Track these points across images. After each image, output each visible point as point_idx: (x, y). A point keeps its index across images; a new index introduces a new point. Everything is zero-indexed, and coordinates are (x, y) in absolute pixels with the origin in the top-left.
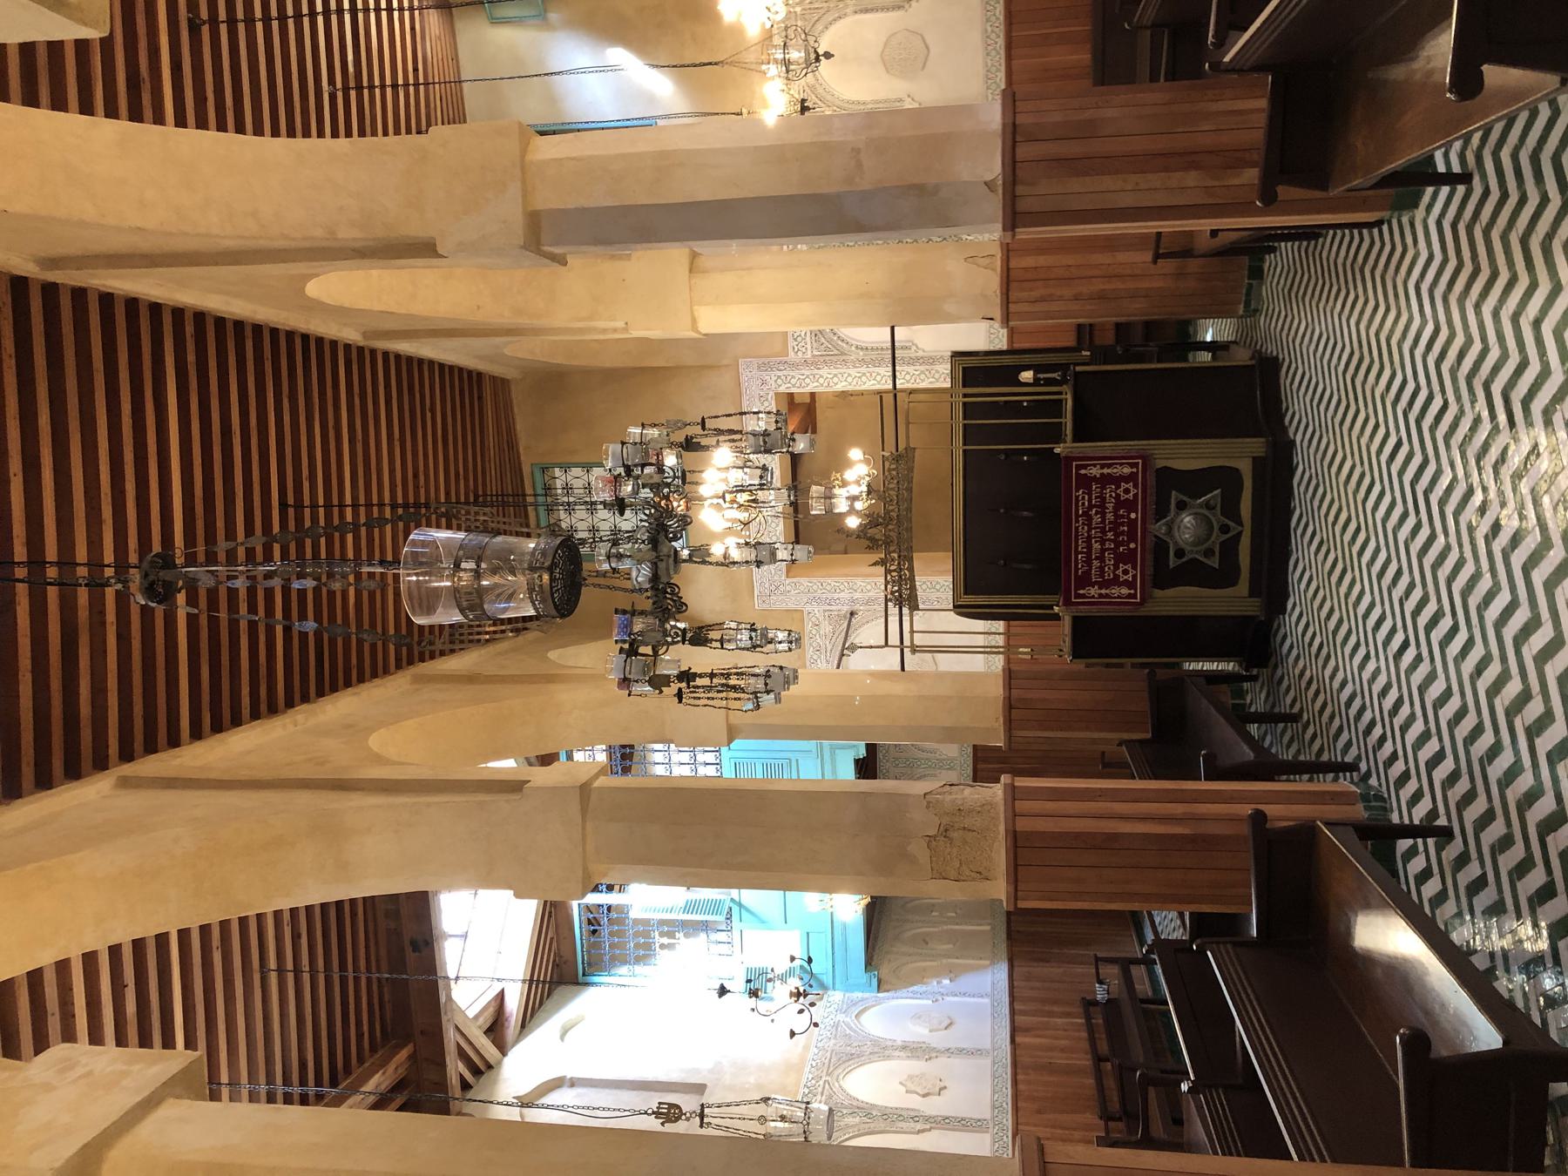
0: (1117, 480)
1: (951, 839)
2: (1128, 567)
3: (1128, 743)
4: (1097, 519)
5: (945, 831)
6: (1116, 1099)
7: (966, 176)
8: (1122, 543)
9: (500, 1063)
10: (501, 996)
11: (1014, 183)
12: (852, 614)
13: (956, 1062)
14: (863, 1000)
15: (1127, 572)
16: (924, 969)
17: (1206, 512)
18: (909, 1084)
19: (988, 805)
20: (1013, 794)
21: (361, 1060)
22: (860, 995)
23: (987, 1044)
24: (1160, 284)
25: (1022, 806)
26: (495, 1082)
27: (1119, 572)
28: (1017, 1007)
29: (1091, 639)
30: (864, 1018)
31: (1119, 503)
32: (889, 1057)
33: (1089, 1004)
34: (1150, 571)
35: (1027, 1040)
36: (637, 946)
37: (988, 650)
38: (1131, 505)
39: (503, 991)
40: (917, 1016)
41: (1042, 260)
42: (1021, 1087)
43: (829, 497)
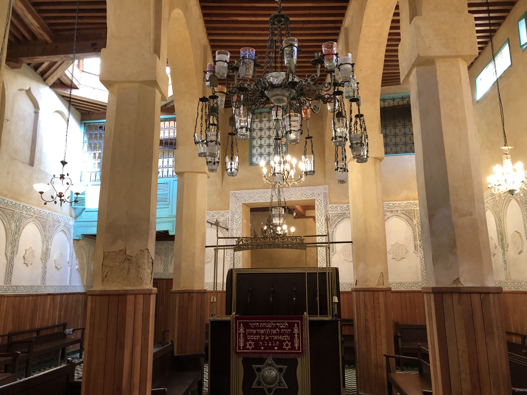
0: (292, 341)
1: (124, 262)
2: (253, 346)
3: (173, 345)
4: (274, 332)
5: (128, 259)
6: (18, 339)
7: (462, 269)
8: (263, 343)
9: (47, 84)
10: (76, 88)
11: (364, 291)
12: (227, 229)
13: (40, 271)
14: (70, 233)
15: (250, 346)
16: (83, 258)
17: (278, 381)
18: (29, 251)
19: (140, 279)
20: (147, 294)
21: (45, 18)
22: (72, 232)
23: (48, 283)
24: (373, 357)
25: (140, 298)
26: (38, 81)
27: (250, 342)
28: (64, 296)
29: (219, 329)
30: (62, 234)
31: (281, 342)
32: (43, 242)
33: (65, 326)
34: (251, 356)
35: (48, 302)
36: (95, 144)
37: (215, 284)
38: (280, 347)
39: (78, 88)
40: (61, 255)
41: (382, 306)
42: (26, 298)
43: (280, 216)
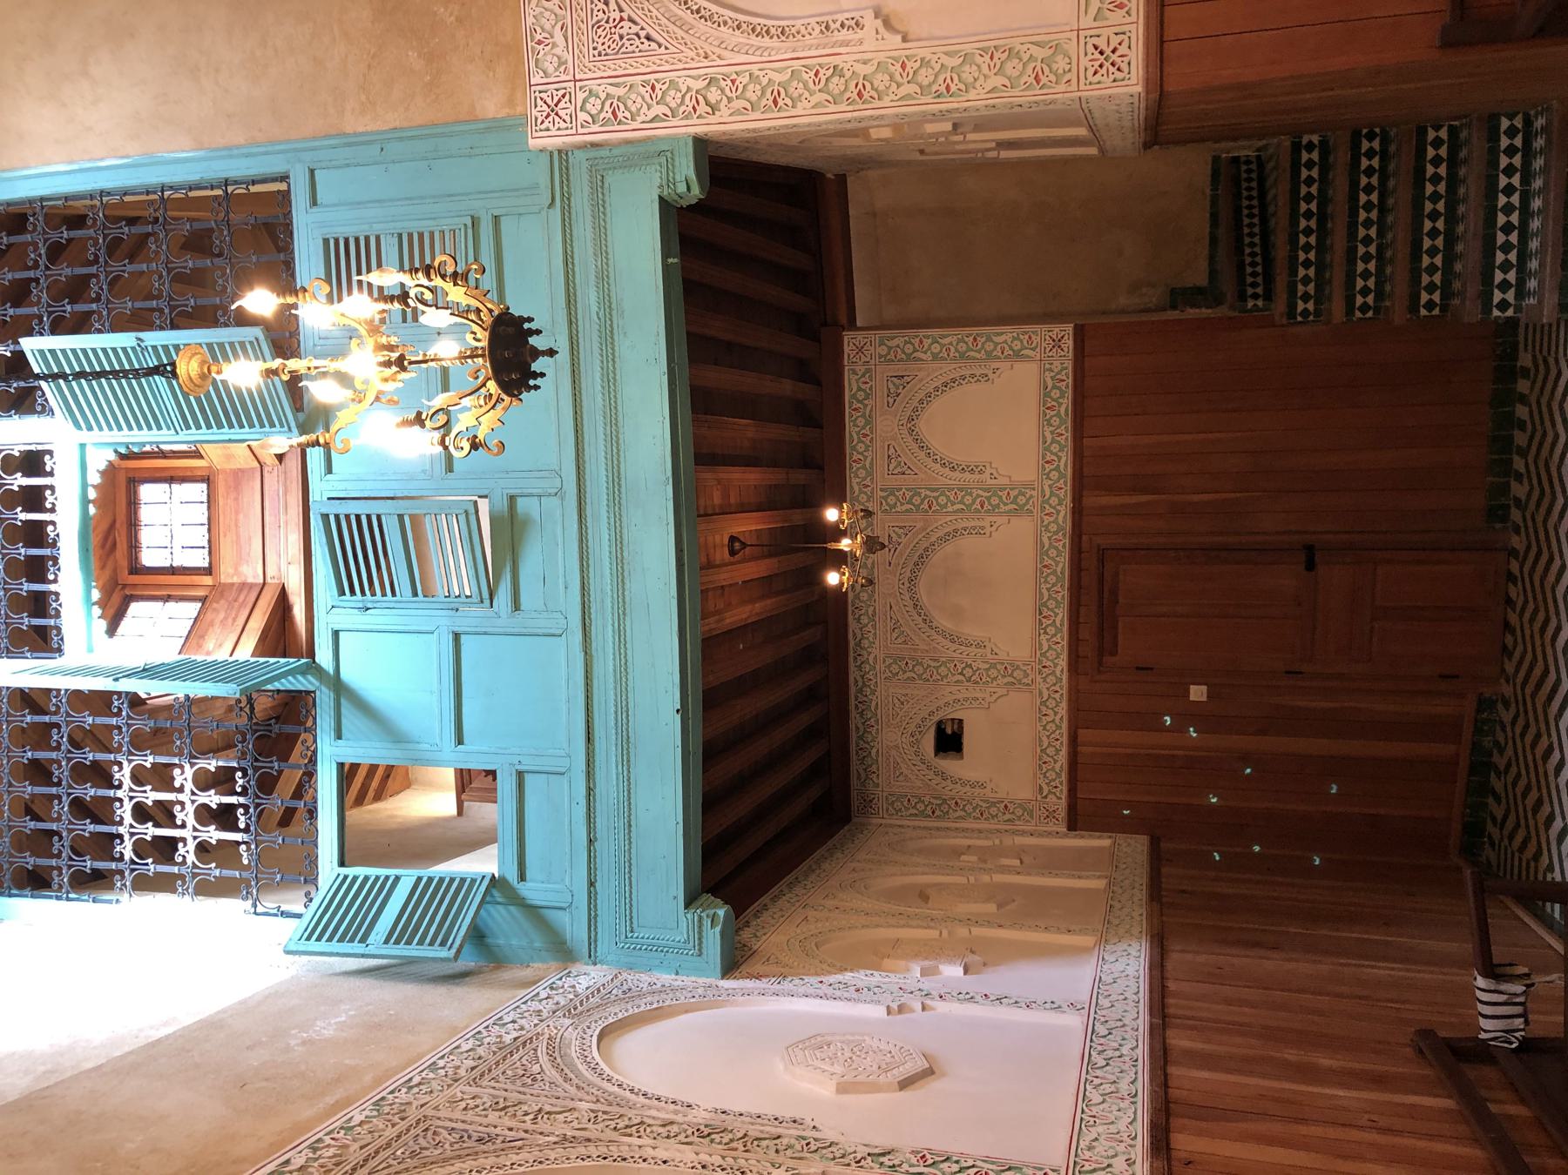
16: (897, 942)
28: (1179, 1041)
33: (1456, 1056)
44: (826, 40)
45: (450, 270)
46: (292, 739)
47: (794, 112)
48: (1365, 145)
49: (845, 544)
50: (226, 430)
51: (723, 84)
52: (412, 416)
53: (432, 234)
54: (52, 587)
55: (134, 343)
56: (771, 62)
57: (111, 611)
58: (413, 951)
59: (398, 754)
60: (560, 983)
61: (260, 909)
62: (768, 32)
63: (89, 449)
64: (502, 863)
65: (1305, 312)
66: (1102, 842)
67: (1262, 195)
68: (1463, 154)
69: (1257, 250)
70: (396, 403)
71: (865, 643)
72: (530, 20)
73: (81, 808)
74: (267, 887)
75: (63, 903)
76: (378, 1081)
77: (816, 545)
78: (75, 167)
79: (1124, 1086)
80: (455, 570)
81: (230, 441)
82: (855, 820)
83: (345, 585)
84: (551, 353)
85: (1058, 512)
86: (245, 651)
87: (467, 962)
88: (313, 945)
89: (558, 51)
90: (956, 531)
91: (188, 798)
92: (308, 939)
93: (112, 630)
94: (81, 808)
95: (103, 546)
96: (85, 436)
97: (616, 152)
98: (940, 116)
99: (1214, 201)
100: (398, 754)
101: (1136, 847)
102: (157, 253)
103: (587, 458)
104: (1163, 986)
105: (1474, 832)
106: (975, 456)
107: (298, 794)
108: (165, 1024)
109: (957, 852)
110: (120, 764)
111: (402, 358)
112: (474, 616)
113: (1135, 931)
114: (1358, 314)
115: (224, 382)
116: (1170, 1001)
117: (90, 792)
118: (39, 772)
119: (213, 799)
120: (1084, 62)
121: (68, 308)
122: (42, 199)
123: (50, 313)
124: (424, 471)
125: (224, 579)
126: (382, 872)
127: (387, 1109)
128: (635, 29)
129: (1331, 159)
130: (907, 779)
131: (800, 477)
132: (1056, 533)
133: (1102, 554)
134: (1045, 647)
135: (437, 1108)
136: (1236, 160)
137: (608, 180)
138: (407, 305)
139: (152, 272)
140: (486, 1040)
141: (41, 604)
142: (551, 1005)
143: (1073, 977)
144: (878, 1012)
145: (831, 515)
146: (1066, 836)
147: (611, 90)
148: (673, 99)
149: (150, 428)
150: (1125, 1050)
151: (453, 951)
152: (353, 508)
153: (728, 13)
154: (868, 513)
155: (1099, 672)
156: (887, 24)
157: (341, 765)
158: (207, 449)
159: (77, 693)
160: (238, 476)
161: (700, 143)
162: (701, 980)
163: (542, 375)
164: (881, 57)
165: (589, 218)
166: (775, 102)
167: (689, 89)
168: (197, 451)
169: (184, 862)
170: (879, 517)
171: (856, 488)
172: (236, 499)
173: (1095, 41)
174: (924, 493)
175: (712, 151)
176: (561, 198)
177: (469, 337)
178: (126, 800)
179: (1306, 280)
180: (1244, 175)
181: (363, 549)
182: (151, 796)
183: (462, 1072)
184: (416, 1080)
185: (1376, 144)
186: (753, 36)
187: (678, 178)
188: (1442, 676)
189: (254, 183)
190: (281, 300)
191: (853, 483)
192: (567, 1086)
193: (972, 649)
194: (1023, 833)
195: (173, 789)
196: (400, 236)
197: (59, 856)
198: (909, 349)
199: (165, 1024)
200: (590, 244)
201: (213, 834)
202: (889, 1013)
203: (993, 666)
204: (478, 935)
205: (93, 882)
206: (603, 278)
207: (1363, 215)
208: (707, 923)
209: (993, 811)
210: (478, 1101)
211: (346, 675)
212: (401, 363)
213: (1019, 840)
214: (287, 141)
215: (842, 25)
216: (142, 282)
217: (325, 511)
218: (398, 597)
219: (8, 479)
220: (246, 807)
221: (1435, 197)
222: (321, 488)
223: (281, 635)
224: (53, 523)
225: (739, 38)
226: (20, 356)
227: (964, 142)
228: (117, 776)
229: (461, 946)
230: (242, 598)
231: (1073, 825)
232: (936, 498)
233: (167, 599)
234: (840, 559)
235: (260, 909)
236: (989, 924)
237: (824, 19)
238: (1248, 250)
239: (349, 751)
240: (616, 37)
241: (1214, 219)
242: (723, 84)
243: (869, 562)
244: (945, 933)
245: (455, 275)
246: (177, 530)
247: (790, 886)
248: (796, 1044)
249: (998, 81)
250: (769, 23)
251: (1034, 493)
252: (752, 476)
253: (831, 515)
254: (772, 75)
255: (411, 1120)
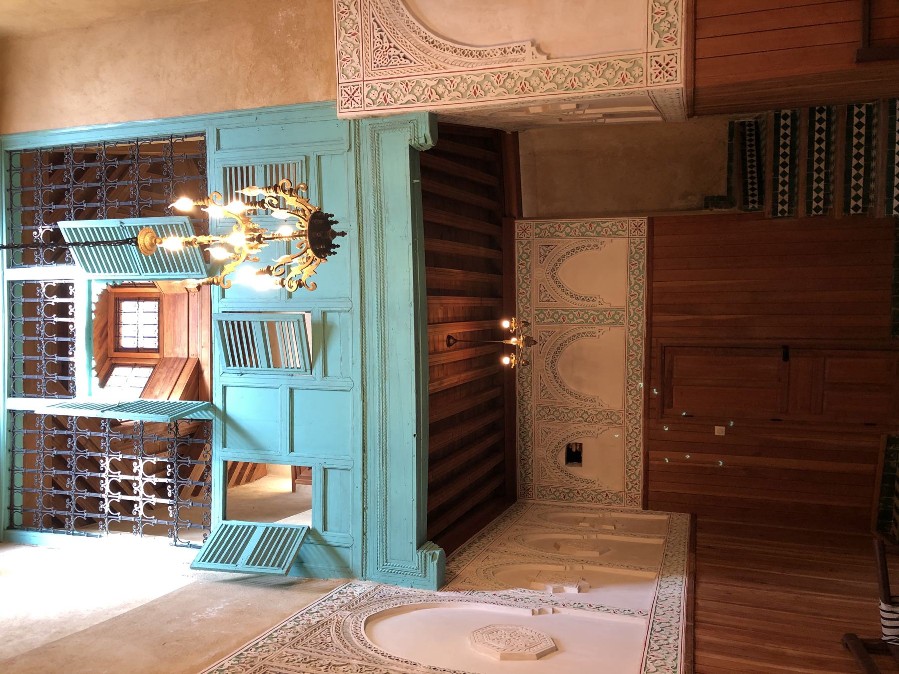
11: (695, 39)
16: (540, 572)
28: (703, 636)
44: (503, 59)
45: (287, 187)
46: (201, 447)
47: (485, 99)
48: (818, 116)
49: (513, 341)
50: (167, 273)
51: (446, 83)
52: (265, 269)
53: (283, 166)
54: (71, 359)
55: (119, 225)
56: (472, 71)
57: (103, 373)
58: (262, 569)
59: (257, 456)
60: (345, 590)
61: (178, 543)
62: (471, 54)
63: (93, 283)
64: (314, 521)
65: (783, 211)
66: (663, 517)
67: (758, 141)
68: (875, 121)
69: (755, 175)
70: (258, 260)
71: (526, 398)
72: (340, 48)
73: (83, 483)
74: (183, 530)
75: (70, 536)
76: (239, 644)
77: (496, 341)
78: (91, 128)
79: (669, 662)
80: (293, 354)
81: (169, 279)
82: (518, 500)
83: (231, 360)
84: (343, 234)
85: (638, 324)
86: (176, 397)
87: (293, 577)
88: (207, 565)
89: (354, 64)
90: (579, 334)
91: (141, 479)
92: (204, 561)
93: (103, 384)
94: (83, 483)
95: (101, 335)
96: (91, 275)
97: (385, 120)
98: (569, 101)
99: (730, 147)
100: (257, 456)
101: (683, 520)
102: (133, 175)
103: (366, 291)
104: (695, 603)
105: (885, 516)
106: (590, 292)
107: (202, 479)
108: (123, 607)
109: (577, 521)
110: (104, 459)
111: (260, 236)
112: (302, 379)
113: (680, 570)
114: (814, 212)
115: (162, 249)
116: (699, 612)
117: (88, 474)
118: (60, 462)
119: (154, 480)
120: (650, 70)
121: (85, 205)
122: (72, 146)
123: (75, 208)
124: (276, 297)
125: (166, 355)
126: (247, 524)
127: (243, 660)
128: (398, 52)
129: (798, 123)
130: (550, 478)
131: (488, 302)
132: (636, 336)
133: (664, 350)
134: (630, 403)
135: (271, 661)
136: (743, 124)
137: (381, 136)
138: (264, 207)
139: (129, 186)
140: (301, 622)
141: (65, 368)
142: (339, 603)
143: (643, 596)
144: (527, 613)
145: (506, 324)
146: (641, 513)
147: (384, 86)
148: (418, 91)
149: (126, 272)
150: (671, 641)
151: (285, 570)
152: (235, 318)
153: (449, 44)
154: (527, 324)
155: (662, 418)
156: (539, 49)
157: (225, 463)
158: (159, 283)
159: (83, 418)
160: (175, 297)
161: (433, 116)
162: (425, 592)
163: (338, 246)
164: (535, 68)
165: (370, 158)
166: (475, 93)
167: (427, 86)
168: (153, 284)
169: (137, 515)
170: (534, 325)
171: (521, 309)
172: (174, 311)
173: (656, 59)
174: (560, 312)
175: (440, 120)
176: (355, 146)
177: (298, 225)
178: (107, 479)
179: (783, 193)
180: (748, 133)
181: (241, 341)
182: (120, 477)
183: (287, 640)
184: (261, 644)
185: (824, 116)
186: (463, 56)
187: (420, 135)
188: (866, 424)
189: (186, 137)
190: (195, 204)
191: (520, 306)
192: (346, 650)
193: (588, 403)
194: (617, 511)
195: (132, 474)
196: (265, 166)
197: (69, 510)
198: (552, 230)
199: (123, 607)
200: (370, 172)
201: (154, 500)
202: (533, 614)
203: (600, 412)
204: (299, 561)
205: (87, 525)
206: (377, 191)
207: (816, 156)
208: (429, 558)
209: (599, 497)
210: (295, 657)
211: (229, 411)
212: (259, 239)
213: (615, 515)
214: (206, 114)
215: (513, 50)
216: (126, 190)
217: (220, 319)
218: (260, 368)
219: (49, 299)
220: (172, 485)
221: (859, 146)
222: (219, 306)
223: (197, 388)
224: (73, 323)
225: (455, 57)
226: (58, 231)
227: (584, 114)
228: (102, 465)
229: (289, 567)
230: (175, 366)
231: (646, 507)
232: (567, 315)
233: (134, 366)
234: (511, 350)
235: (178, 543)
236: (594, 563)
237: (503, 47)
238: (749, 175)
239: (230, 454)
240: (387, 57)
241: (730, 158)
242: (446, 83)
243: (528, 352)
244: (568, 568)
245: (291, 190)
246: (141, 327)
247: (479, 538)
248: (478, 630)
249: (601, 81)
250: (472, 49)
251: (624, 313)
252: (460, 302)
253: (506, 324)
254: (473, 78)
255: (257, 667)
